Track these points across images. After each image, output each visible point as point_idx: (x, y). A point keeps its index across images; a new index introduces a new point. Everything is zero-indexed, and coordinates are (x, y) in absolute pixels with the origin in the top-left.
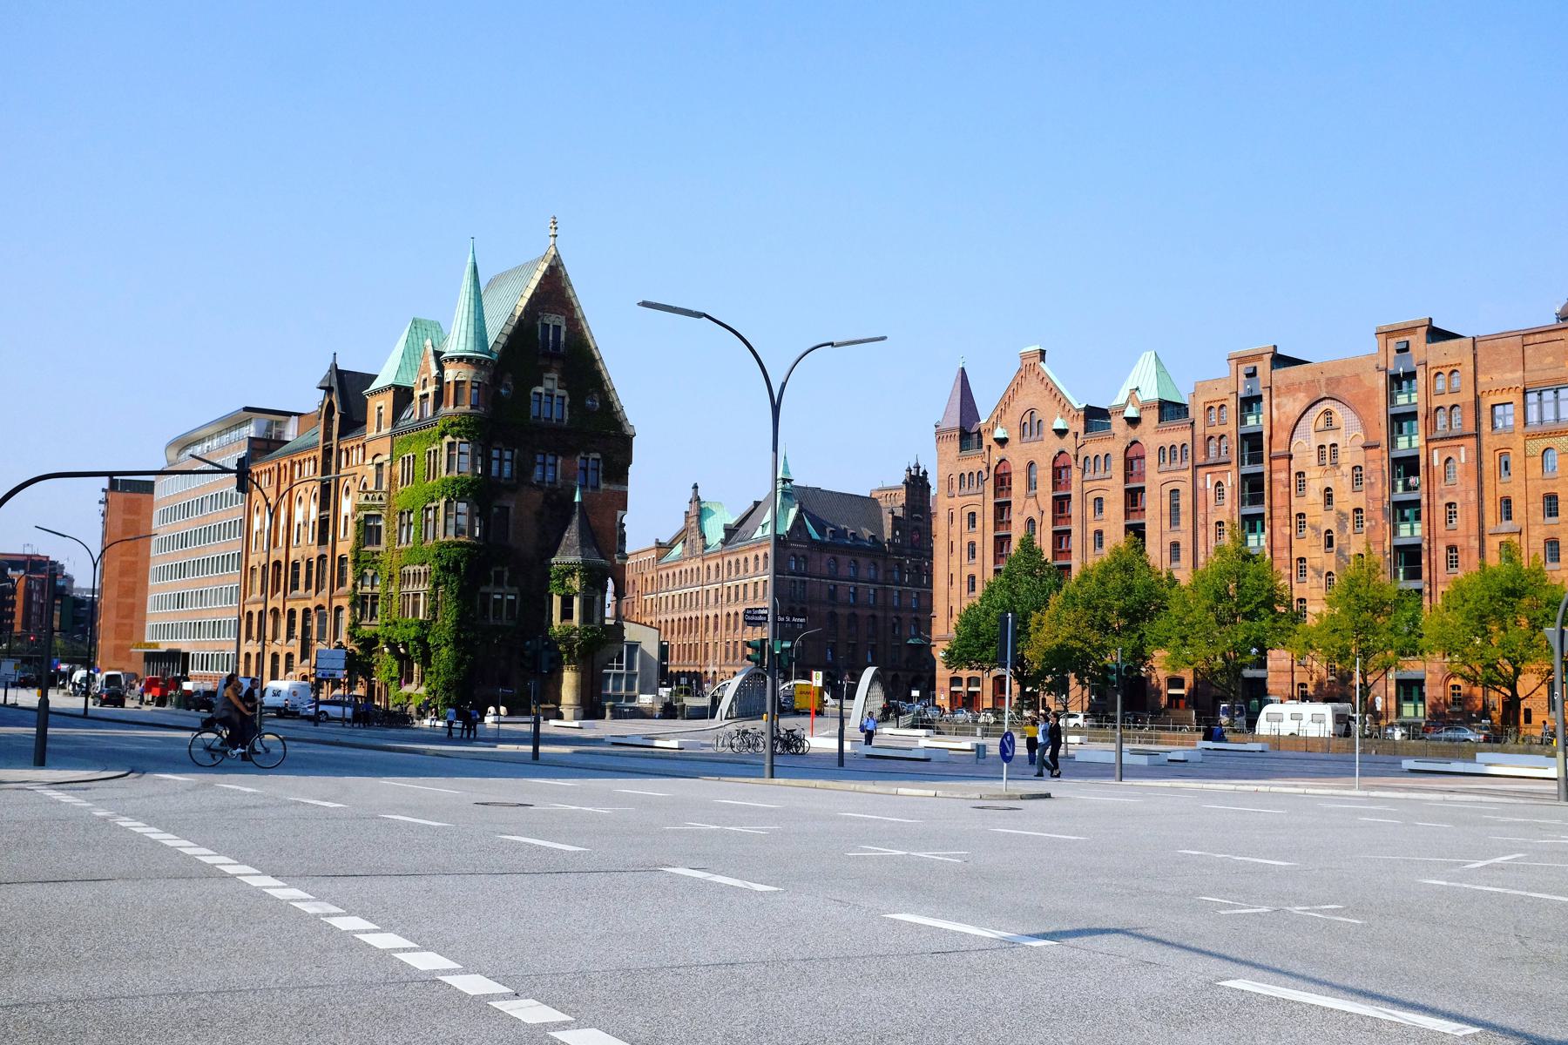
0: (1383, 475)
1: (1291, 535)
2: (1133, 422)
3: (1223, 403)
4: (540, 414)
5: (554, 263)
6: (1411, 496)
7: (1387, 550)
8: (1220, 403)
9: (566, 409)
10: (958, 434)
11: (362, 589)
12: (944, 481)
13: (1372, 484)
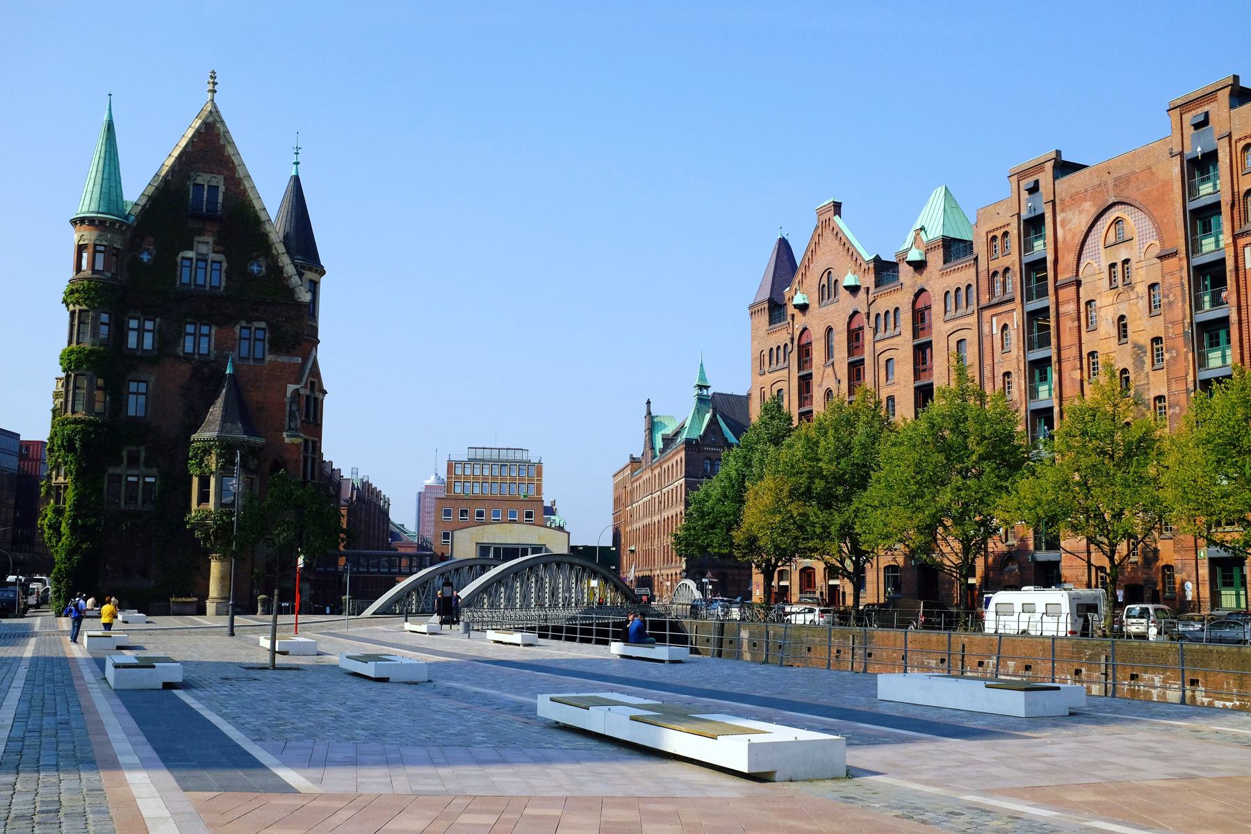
0: (1183, 289)
1: (1082, 381)
2: (919, 266)
3: (1006, 229)
4: (220, 284)
5: (210, 120)
6: (1218, 313)
7: (1191, 387)
8: (1003, 230)
9: (223, 275)
10: (766, 306)
11: (56, 479)
12: (757, 358)
13: (1170, 303)
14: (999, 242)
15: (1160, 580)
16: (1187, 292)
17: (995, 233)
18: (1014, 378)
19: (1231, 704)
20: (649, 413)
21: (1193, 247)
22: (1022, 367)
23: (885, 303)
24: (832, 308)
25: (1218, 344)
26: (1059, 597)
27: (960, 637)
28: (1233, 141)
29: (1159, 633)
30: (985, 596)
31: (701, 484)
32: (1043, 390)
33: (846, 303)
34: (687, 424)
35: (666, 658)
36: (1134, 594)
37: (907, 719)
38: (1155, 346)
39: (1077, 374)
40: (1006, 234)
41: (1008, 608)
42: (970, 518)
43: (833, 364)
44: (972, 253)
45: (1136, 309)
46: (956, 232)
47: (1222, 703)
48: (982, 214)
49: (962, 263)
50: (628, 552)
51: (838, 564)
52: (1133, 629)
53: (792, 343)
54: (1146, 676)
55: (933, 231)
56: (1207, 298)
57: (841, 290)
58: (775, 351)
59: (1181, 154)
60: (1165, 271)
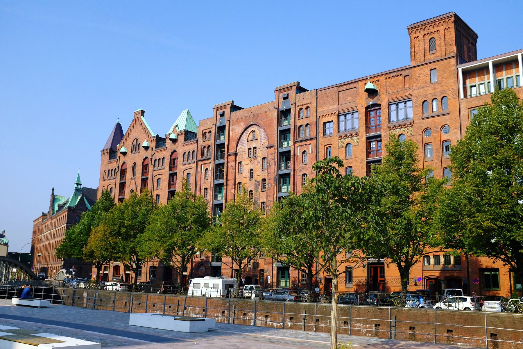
2: (174, 141)
3: (210, 130)
7: (275, 199)
8: (209, 130)
10: (109, 151)
13: (270, 166)
14: (207, 134)
15: (259, 275)
16: (276, 162)
17: (206, 131)
18: (209, 190)
19: (279, 324)
20: (53, 194)
21: (280, 145)
22: (212, 186)
23: (159, 155)
24: (137, 155)
25: (286, 183)
26: (218, 281)
27: (178, 297)
28: (296, 106)
29: (256, 296)
30: (190, 280)
31: (71, 227)
32: (219, 196)
33: (143, 153)
34: (70, 200)
35: (38, 305)
36: (249, 281)
37: (139, 333)
38: (263, 182)
39: (233, 191)
40: (210, 132)
41: (198, 285)
42: (186, 247)
43: (135, 179)
44: (196, 138)
45: (257, 166)
46: (191, 129)
47: (276, 324)
48: (202, 122)
49: (193, 141)
50: (38, 256)
51: (129, 265)
52: (247, 295)
53: (118, 168)
54: (249, 314)
55: (182, 127)
56: (283, 165)
57: (141, 148)
58: (110, 171)
59: (278, 108)
60: (269, 153)
